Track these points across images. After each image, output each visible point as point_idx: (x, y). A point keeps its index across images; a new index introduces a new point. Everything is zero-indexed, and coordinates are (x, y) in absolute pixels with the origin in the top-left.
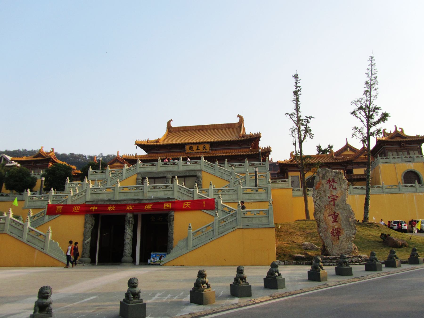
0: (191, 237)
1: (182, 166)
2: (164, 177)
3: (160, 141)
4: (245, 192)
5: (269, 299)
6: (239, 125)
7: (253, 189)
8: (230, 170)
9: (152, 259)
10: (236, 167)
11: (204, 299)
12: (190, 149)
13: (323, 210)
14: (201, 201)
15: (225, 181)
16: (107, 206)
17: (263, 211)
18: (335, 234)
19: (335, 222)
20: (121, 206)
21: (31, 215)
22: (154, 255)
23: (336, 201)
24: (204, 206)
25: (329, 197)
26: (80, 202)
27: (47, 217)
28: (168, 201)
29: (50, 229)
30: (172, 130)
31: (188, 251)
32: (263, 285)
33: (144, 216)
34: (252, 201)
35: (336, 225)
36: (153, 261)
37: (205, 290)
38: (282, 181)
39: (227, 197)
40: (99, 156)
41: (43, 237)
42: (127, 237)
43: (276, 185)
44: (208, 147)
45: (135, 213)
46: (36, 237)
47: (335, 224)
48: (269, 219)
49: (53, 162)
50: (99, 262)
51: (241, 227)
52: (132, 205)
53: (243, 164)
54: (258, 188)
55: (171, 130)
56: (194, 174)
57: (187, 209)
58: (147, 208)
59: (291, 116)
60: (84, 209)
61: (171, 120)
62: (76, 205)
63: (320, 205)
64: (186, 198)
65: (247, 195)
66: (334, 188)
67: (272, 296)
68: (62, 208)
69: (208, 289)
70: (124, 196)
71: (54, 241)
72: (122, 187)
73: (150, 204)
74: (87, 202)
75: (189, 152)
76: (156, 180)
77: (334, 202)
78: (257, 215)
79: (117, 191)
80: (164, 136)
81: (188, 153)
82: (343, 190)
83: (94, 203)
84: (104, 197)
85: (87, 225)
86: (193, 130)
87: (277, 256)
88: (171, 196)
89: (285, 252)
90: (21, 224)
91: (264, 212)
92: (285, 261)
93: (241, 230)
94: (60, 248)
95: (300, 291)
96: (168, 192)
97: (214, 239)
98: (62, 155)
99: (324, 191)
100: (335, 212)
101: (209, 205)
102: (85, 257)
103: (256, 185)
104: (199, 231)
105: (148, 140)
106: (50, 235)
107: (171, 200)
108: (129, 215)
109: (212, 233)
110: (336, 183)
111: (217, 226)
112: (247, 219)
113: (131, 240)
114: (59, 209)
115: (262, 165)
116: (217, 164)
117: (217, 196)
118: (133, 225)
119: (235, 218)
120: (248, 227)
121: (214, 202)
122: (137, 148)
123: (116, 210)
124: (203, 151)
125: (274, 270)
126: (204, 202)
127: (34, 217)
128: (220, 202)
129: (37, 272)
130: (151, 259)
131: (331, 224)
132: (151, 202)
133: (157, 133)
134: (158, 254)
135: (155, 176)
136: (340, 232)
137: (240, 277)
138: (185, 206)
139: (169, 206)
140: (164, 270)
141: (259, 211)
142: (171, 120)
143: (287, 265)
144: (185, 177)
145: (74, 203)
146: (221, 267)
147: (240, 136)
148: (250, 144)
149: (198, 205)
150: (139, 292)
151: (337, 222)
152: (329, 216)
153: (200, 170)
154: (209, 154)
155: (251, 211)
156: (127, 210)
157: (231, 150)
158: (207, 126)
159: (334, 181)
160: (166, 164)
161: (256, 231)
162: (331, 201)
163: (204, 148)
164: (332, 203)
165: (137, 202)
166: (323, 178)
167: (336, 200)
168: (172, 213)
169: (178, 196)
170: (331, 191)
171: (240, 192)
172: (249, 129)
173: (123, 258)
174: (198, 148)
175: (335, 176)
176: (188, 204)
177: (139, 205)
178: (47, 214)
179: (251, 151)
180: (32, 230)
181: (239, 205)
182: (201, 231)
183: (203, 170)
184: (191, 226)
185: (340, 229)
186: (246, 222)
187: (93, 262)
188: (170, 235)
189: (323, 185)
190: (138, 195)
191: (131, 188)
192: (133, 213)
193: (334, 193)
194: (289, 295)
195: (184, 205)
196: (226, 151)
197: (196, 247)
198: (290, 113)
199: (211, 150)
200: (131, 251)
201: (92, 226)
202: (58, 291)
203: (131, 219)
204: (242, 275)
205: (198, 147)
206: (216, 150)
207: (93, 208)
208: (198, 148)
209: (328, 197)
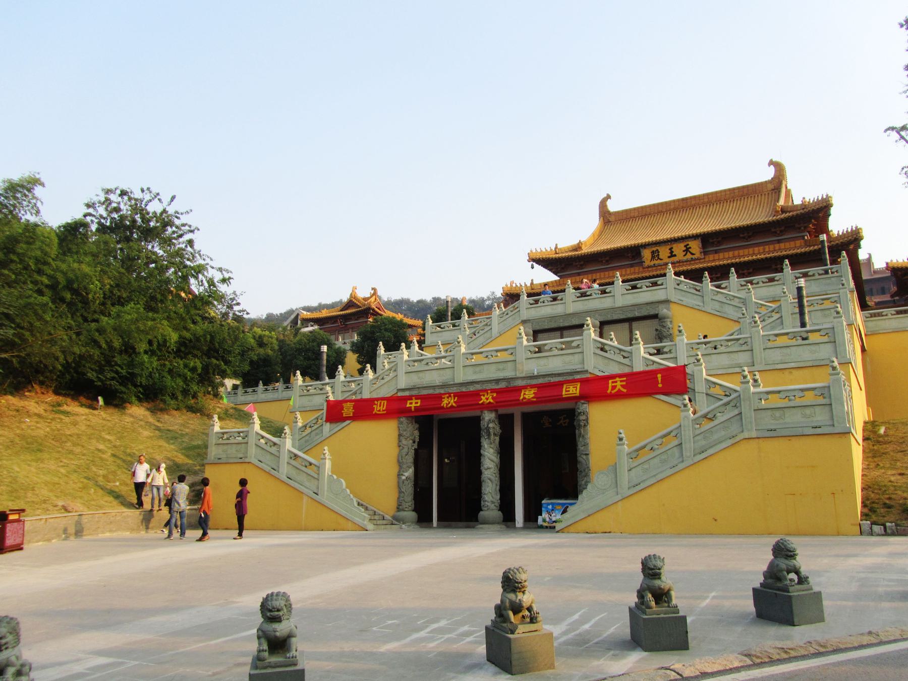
0: (625, 463)
1: (621, 296)
3: (583, 247)
4: (770, 344)
5: (736, 664)
6: (777, 184)
7: (794, 336)
8: (742, 294)
9: (545, 515)
10: (761, 284)
11: (515, 657)
12: (653, 258)
14: (654, 373)
15: (732, 323)
16: (439, 397)
17: (814, 389)
20: (468, 396)
21: (300, 424)
22: (550, 507)
24: (660, 385)
26: (387, 391)
27: (327, 427)
28: (571, 378)
29: (326, 451)
30: (612, 219)
31: (619, 497)
32: (749, 605)
33: (525, 416)
34: (793, 365)
36: (548, 519)
37: (521, 628)
38: (898, 313)
39: (724, 360)
40: (489, 299)
41: (315, 468)
42: (486, 466)
43: (880, 323)
44: (695, 246)
45: (502, 411)
46: (304, 468)
48: (832, 410)
49: (375, 314)
50: (439, 520)
51: (754, 434)
52: (493, 391)
53: (777, 276)
54: (808, 332)
55: (609, 219)
56: (652, 312)
57: (619, 396)
58: (524, 398)
59: (903, 133)
60: (396, 407)
61: (608, 197)
62: (378, 399)
64: (614, 369)
65: (778, 351)
67: (748, 655)
68: (354, 407)
69: (533, 627)
70: (475, 373)
71: (335, 477)
72: (508, 357)
73: (532, 386)
74: (399, 390)
75: (652, 263)
76: (565, 333)
78: (798, 402)
79: (461, 362)
80: (593, 234)
81: (649, 267)
83: (414, 393)
84: (433, 379)
85: (404, 442)
86: (660, 212)
87: (866, 510)
88: (578, 367)
89: (890, 499)
90: (275, 444)
91: (816, 392)
92: (888, 524)
93: (753, 443)
94: (348, 491)
95: (866, 640)
96: (571, 357)
97: (681, 466)
98: (419, 302)
101: (674, 382)
102: (403, 510)
103: (803, 325)
104: (644, 447)
105: (556, 248)
106: (328, 464)
107: (578, 377)
108: (488, 417)
109: (676, 451)
111: (687, 434)
112: (769, 412)
113: (497, 471)
114: (348, 410)
115: (830, 275)
116: (708, 285)
117: (693, 360)
118: (497, 439)
119: (736, 412)
120: (772, 434)
121: (685, 373)
122: (532, 267)
123: (458, 406)
124: (685, 258)
125: (784, 566)
126: (659, 376)
127: (305, 426)
128: (701, 374)
129: (287, 545)
130: (544, 515)
132: (534, 382)
133: (578, 231)
134: (559, 504)
135: (561, 325)
137: (653, 589)
138: (614, 387)
139: (573, 390)
140: (544, 546)
141: (802, 390)
142: (608, 197)
143: (893, 534)
144: (630, 320)
145: (375, 396)
146: (693, 540)
147: (777, 212)
148: (805, 227)
149: (641, 385)
150: (290, 636)
153: (667, 302)
154: (701, 263)
155: (779, 392)
156: (483, 404)
157: (756, 249)
158: (695, 198)
160: (584, 295)
161: (797, 443)
163: (687, 250)
165: (502, 385)
168: (583, 407)
169: (595, 366)
171: (758, 346)
172: (801, 191)
173: (481, 513)
174: (672, 252)
176: (619, 384)
177: (508, 392)
178: (327, 421)
179: (807, 244)
180: (296, 456)
181: (745, 377)
182: (649, 447)
183: (673, 300)
184: (623, 435)
186: (768, 421)
187: (423, 519)
188: (581, 458)
190: (480, 372)
191: (490, 353)
192: (496, 411)
194: (818, 654)
195: (610, 385)
196: (741, 252)
197: (637, 488)
198: (899, 125)
199: (705, 253)
200: (499, 497)
201: (414, 442)
202: (238, 600)
203: (491, 425)
204: (657, 583)
205: (671, 249)
206: (716, 252)
207: (413, 404)
208: (672, 252)
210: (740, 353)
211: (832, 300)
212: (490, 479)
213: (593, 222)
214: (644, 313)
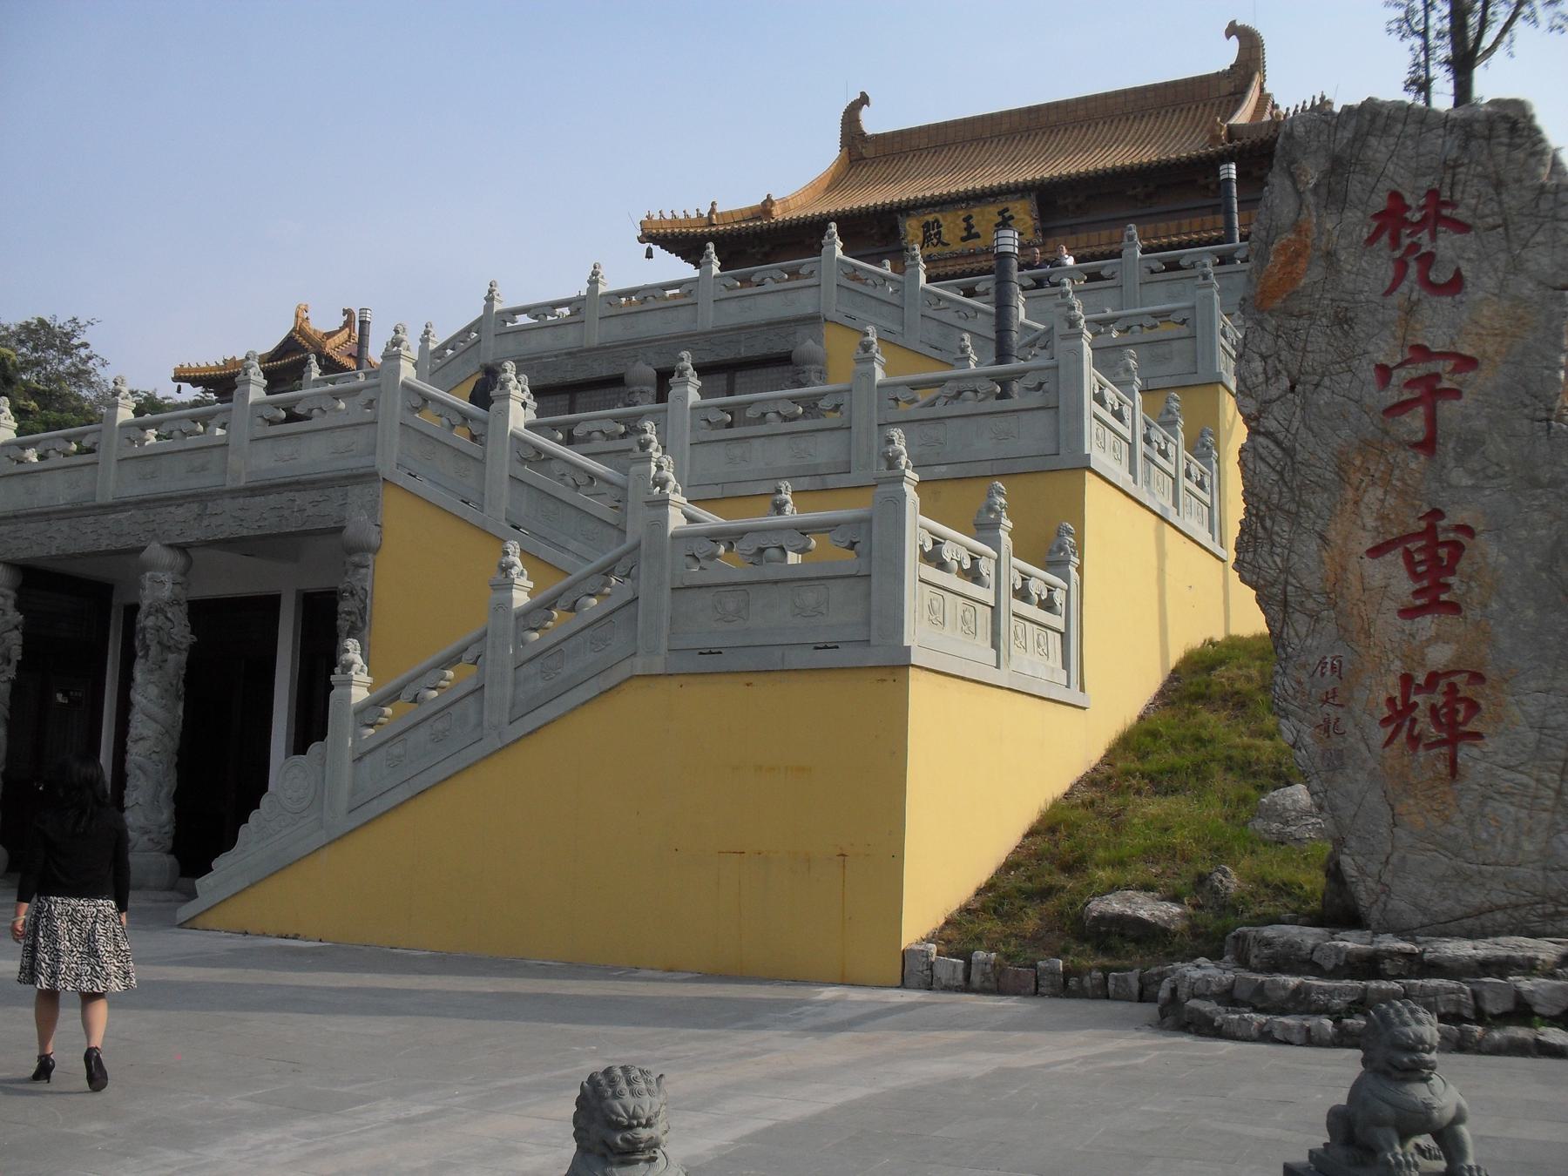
2: (617, 381)
13: (1318, 500)
18: (1424, 724)
19: (1435, 606)
21: (520, 598)
23: (1446, 409)
25: (1384, 372)
30: (868, 152)
35: (1437, 638)
47: (1427, 624)
56: (779, 347)
61: (864, 100)
63: (1289, 452)
66: (1439, 276)
77: (1431, 420)
82: (1528, 288)
99: (1343, 321)
100: (1437, 514)
105: (712, 211)
110: (1462, 227)
120: (707, 662)
122: (649, 255)
131: (1388, 625)
135: (569, 378)
136: (1474, 707)
142: (864, 100)
143: (997, 986)
151: (1454, 608)
152: (1376, 552)
159: (1438, 212)
162: (1403, 407)
164: (1414, 423)
166: (1333, 195)
167: (1456, 394)
170: (1411, 310)
174: (969, 228)
175: (1452, 166)
183: (831, 315)
185: (1477, 677)
189: (1330, 255)
193: (1438, 326)
205: (967, 219)
208: (969, 228)
209: (1370, 374)
210: (820, 437)
211: (1177, 317)
212: (140, 768)
213: (825, 151)
214: (759, 348)
